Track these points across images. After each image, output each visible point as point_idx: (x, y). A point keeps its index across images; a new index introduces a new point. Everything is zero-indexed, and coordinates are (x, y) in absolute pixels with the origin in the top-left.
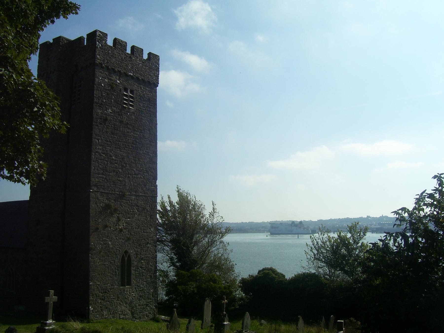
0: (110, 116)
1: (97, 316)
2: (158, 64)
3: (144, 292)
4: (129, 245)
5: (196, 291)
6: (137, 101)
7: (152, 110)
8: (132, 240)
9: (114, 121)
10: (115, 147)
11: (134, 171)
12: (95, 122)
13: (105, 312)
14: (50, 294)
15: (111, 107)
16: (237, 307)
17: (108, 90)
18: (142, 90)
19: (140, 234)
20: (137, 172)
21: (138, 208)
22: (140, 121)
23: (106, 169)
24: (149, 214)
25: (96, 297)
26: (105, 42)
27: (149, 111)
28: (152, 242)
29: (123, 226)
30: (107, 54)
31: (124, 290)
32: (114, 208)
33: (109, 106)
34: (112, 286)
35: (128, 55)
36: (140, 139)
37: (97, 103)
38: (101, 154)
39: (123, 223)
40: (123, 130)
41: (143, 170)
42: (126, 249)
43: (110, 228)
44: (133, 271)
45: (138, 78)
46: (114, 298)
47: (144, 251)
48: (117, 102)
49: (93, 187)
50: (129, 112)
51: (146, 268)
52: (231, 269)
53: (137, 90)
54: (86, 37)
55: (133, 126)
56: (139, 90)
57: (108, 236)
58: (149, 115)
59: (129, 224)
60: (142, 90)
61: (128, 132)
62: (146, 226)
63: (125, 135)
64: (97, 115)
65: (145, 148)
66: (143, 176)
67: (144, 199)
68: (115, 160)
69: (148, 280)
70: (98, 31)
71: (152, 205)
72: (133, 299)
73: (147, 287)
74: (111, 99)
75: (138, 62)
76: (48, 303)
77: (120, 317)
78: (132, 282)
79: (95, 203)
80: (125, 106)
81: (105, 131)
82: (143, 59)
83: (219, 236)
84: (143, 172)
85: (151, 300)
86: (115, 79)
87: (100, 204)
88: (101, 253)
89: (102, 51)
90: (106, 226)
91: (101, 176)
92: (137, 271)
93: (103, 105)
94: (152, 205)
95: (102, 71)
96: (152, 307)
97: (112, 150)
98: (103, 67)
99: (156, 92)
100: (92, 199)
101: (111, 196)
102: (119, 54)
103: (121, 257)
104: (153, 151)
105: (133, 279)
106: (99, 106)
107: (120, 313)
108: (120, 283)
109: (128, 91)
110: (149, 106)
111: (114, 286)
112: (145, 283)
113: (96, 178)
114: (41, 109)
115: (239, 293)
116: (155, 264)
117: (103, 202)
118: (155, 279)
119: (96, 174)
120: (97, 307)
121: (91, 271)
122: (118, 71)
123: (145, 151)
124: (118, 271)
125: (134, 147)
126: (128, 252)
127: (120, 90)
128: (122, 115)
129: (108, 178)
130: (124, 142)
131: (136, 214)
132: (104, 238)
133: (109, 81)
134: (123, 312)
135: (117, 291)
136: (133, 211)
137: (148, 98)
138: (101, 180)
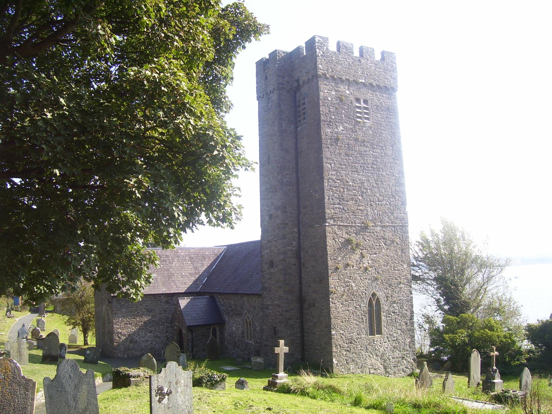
0: (342, 134)
1: (343, 370)
2: (394, 63)
3: (399, 343)
4: (377, 286)
5: (467, 341)
6: (374, 112)
9: (347, 140)
10: (351, 171)
12: (325, 144)
13: (351, 366)
14: (280, 345)
15: (342, 123)
16: (523, 362)
17: (337, 103)
18: (378, 98)
19: (390, 272)
20: (381, 198)
22: (379, 136)
23: (343, 197)
24: (400, 248)
25: (341, 348)
26: (327, 48)
27: (390, 122)
28: (405, 281)
29: (369, 263)
30: (330, 61)
31: (374, 341)
32: (356, 243)
33: (340, 122)
34: (359, 335)
35: (357, 58)
36: (382, 158)
37: (325, 121)
38: (335, 180)
40: (359, 149)
41: (388, 194)
42: (373, 291)
43: (353, 267)
44: (383, 317)
45: (371, 84)
46: (362, 350)
47: (396, 293)
48: (349, 116)
50: (365, 127)
52: (515, 313)
53: (371, 99)
54: (304, 45)
55: (372, 143)
57: (351, 277)
59: (375, 261)
60: (378, 98)
61: (366, 151)
62: (396, 262)
64: (327, 136)
65: (389, 168)
66: (388, 202)
69: (402, 327)
70: (317, 37)
72: (385, 350)
73: (402, 336)
74: (341, 114)
75: (369, 66)
77: (370, 372)
78: (383, 331)
79: (332, 238)
80: (358, 120)
81: (337, 153)
82: (375, 61)
83: (496, 270)
85: (408, 352)
86: (344, 90)
88: (343, 297)
89: (324, 60)
90: (348, 265)
91: (337, 206)
92: (389, 317)
93: (331, 122)
95: (327, 82)
96: (409, 360)
97: (348, 175)
98: (328, 77)
102: (345, 59)
103: (368, 302)
104: (399, 171)
105: (384, 326)
106: (327, 124)
107: (369, 367)
108: (368, 331)
111: (361, 335)
112: (399, 331)
113: (331, 209)
114: (221, 152)
115: (526, 345)
116: (411, 308)
117: (342, 237)
118: (411, 326)
119: (331, 204)
121: (332, 318)
122: (346, 79)
123: (389, 172)
124: (365, 317)
125: (374, 168)
128: (356, 131)
129: (346, 208)
131: (383, 249)
132: (346, 280)
133: (337, 93)
134: (373, 366)
135: (365, 341)
136: (379, 246)
137: (386, 106)
138: (337, 211)
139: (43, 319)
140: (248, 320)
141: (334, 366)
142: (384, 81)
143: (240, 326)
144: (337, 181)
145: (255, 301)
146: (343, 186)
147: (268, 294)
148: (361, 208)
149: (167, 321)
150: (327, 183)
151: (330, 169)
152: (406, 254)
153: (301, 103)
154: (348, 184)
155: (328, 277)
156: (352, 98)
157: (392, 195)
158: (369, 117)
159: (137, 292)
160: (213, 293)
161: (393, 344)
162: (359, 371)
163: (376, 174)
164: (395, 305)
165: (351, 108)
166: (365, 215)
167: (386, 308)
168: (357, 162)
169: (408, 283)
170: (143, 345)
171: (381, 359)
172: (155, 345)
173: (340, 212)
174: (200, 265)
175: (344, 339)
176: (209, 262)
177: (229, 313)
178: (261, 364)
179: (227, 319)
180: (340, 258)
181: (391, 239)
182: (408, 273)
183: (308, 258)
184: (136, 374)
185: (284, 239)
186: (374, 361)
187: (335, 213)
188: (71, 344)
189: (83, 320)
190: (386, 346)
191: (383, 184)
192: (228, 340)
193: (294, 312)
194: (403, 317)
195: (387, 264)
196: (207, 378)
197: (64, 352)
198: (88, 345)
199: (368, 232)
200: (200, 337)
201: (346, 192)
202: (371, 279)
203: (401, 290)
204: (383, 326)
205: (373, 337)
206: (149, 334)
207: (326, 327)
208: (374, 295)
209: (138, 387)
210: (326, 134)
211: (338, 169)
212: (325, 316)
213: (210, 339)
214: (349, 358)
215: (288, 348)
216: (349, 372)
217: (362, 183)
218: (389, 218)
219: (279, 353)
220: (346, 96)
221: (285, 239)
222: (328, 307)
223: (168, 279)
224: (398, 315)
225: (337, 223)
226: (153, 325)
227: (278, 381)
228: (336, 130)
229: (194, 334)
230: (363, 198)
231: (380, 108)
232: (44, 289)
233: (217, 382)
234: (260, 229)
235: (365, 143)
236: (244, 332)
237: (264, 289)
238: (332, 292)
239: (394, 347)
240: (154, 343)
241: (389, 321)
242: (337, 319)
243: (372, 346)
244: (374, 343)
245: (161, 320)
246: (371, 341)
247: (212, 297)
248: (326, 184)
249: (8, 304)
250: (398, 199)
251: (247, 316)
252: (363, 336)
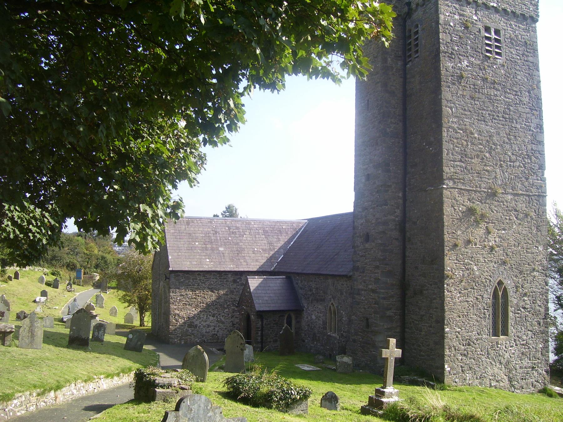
0: (466, 71)
1: (457, 380)
6: (507, 46)
7: (530, 59)
8: (509, 265)
9: (473, 79)
10: (477, 119)
11: (508, 155)
12: (444, 82)
13: (467, 375)
20: (513, 158)
21: (518, 215)
22: (513, 77)
23: (465, 153)
28: (540, 268)
29: (495, 241)
31: (497, 343)
37: (446, 52)
38: (456, 130)
39: (494, 238)
41: (522, 153)
43: (476, 245)
44: (511, 313)
45: (505, 10)
46: (483, 355)
49: (446, 182)
50: (496, 64)
51: (531, 309)
56: (509, 29)
57: (472, 257)
58: (527, 67)
60: (513, 28)
61: (496, 95)
62: (530, 242)
63: (492, 101)
64: (447, 71)
65: (524, 120)
66: (522, 163)
67: (526, 199)
68: (479, 140)
69: (534, 328)
71: (538, 210)
72: (510, 356)
73: (533, 339)
74: (466, 45)
76: (387, 359)
78: (510, 331)
80: (488, 54)
84: (523, 158)
85: (539, 361)
87: (459, 207)
88: (462, 284)
90: (469, 242)
91: (458, 163)
92: (518, 313)
93: (454, 54)
94: (538, 210)
97: (473, 124)
99: (535, 31)
100: (446, 199)
101: (475, 195)
105: (511, 325)
106: (449, 57)
107: (490, 378)
109: (491, 32)
110: (526, 53)
112: (529, 332)
113: (451, 167)
116: (546, 304)
117: (463, 205)
118: (545, 327)
119: (451, 161)
120: (456, 366)
121: (447, 310)
123: (525, 125)
125: (507, 118)
126: (503, 284)
127: (478, 30)
128: (485, 69)
129: (469, 168)
130: (491, 111)
131: (514, 224)
132: (466, 261)
133: (461, 17)
135: (487, 344)
136: (510, 219)
137: (523, 41)
139: (102, 295)
140: (332, 308)
141: (446, 375)
142: (522, 8)
143: (322, 315)
144: (459, 131)
145: (342, 284)
146: (466, 138)
147: (361, 275)
148: (488, 168)
149: (233, 304)
150: (446, 133)
151: (451, 115)
152: (542, 232)
153: (412, 33)
154: (472, 136)
155: (444, 255)
156: (480, 26)
157: (528, 155)
158: (501, 52)
159: (145, 231)
160: (289, 273)
161: (522, 349)
162: (477, 382)
163: (508, 126)
164: (526, 298)
165: (478, 39)
166: (493, 178)
167: (515, 301)
168: (485, 108)
169: (543, 270)
170: (204, 331)
171: (505, 368)
172: (218, 331)
173: (461, 171)
174: (275, 240)
175: (460, 339)
176: (286, 237)
177: (308, 298)
178: (349, 365)
179: (305, 305)
180: (459, 232)
181: (525, 212)
182: (544, 258)
183: (416, 231)
184: (166, 381)
185: (385, 205)
186: (496, 370)
187: (456, 173)
188: (126, 324)
189: (139, 298)
190: (513, 352)
191: (516, 140)
192: (306, 331)
193: (394, 300)
194: (536, 314)
195: (518, 244)
196: (279, 394)
197: (103, 334)
198: (144, 326)
199: (496, 201)
200: (272, 325)
201: (469, 146)
202: (498, 262)
203: (535, 279)
204: (510, 324)
205: (497, 339)
206: (211, 318)
207: (437, 322)
208: (500, 283)
209: (166, 404)
210: (446, 69)
211: (461, 116)
212: (437, 308)
213: (284, 328)
214: (466, 364)
215: (400, 350)
216: (465, 384)
217: (490, 136)
218: (523, 185)
219: (387, 358)
220: (472, 23)
221: (387, 205)
222: (441, 295)
223: (237, 255)
224: (530, 311)
225: (457, 186)
226: (216, 308)
227: (384, 400)
228: (459, 65)
229: (265, 322)
230: (491, 156)
231: (516, 41)
232: (14, 231)
233: (295, 401)
234: (353, 193)
235: (496, 86)
236: (326, 323)
237: (355, 269)
238: (448, 276)
239: (523, 354)
240: (217, 329)
241: (517, 319)
242: (453, 312)
243: (495, 350)
244: (498, 347)
245: (227, 303)
246: (494, 343)
247: (290, 277)
248: (445, 134)
249: (70, 278)
250: (535, 161)
251: (330, 303)
252: (484, 336)
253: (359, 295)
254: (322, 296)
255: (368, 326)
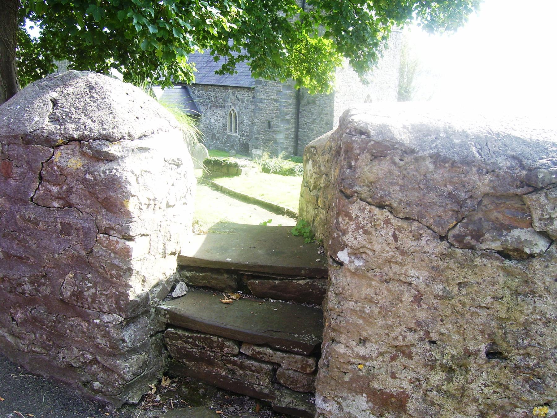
143: (221, 119)
236: (226, 125)
251: (231, 109)
253: (262, 103)
254: (222, 103)
255: (270, 127)
